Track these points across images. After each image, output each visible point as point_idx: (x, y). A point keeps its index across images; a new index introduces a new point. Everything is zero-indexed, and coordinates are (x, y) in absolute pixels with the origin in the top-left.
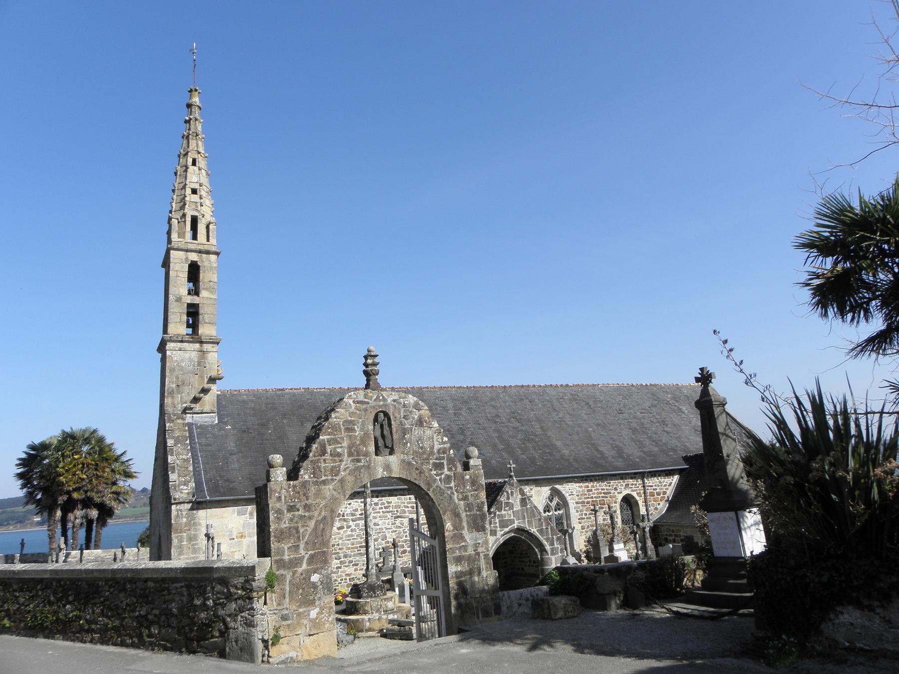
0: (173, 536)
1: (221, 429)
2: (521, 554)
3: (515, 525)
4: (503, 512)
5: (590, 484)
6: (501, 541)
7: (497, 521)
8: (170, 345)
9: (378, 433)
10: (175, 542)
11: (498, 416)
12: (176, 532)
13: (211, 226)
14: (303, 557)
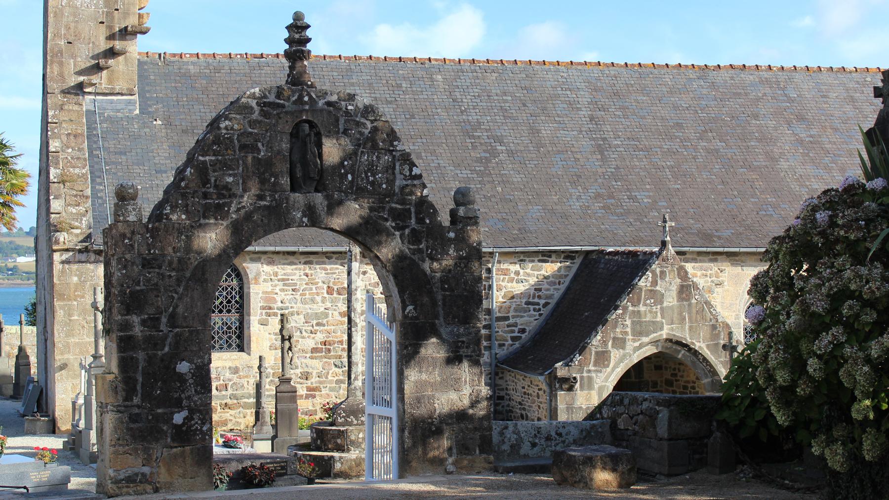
0: (57, 303)
3: (664, 333)
4: (642, 308)
7: (628, 322)
9: (296, 157)
10: (60, 314)
11: (679, 126)
12: (62, 297)
14: (166, 337)
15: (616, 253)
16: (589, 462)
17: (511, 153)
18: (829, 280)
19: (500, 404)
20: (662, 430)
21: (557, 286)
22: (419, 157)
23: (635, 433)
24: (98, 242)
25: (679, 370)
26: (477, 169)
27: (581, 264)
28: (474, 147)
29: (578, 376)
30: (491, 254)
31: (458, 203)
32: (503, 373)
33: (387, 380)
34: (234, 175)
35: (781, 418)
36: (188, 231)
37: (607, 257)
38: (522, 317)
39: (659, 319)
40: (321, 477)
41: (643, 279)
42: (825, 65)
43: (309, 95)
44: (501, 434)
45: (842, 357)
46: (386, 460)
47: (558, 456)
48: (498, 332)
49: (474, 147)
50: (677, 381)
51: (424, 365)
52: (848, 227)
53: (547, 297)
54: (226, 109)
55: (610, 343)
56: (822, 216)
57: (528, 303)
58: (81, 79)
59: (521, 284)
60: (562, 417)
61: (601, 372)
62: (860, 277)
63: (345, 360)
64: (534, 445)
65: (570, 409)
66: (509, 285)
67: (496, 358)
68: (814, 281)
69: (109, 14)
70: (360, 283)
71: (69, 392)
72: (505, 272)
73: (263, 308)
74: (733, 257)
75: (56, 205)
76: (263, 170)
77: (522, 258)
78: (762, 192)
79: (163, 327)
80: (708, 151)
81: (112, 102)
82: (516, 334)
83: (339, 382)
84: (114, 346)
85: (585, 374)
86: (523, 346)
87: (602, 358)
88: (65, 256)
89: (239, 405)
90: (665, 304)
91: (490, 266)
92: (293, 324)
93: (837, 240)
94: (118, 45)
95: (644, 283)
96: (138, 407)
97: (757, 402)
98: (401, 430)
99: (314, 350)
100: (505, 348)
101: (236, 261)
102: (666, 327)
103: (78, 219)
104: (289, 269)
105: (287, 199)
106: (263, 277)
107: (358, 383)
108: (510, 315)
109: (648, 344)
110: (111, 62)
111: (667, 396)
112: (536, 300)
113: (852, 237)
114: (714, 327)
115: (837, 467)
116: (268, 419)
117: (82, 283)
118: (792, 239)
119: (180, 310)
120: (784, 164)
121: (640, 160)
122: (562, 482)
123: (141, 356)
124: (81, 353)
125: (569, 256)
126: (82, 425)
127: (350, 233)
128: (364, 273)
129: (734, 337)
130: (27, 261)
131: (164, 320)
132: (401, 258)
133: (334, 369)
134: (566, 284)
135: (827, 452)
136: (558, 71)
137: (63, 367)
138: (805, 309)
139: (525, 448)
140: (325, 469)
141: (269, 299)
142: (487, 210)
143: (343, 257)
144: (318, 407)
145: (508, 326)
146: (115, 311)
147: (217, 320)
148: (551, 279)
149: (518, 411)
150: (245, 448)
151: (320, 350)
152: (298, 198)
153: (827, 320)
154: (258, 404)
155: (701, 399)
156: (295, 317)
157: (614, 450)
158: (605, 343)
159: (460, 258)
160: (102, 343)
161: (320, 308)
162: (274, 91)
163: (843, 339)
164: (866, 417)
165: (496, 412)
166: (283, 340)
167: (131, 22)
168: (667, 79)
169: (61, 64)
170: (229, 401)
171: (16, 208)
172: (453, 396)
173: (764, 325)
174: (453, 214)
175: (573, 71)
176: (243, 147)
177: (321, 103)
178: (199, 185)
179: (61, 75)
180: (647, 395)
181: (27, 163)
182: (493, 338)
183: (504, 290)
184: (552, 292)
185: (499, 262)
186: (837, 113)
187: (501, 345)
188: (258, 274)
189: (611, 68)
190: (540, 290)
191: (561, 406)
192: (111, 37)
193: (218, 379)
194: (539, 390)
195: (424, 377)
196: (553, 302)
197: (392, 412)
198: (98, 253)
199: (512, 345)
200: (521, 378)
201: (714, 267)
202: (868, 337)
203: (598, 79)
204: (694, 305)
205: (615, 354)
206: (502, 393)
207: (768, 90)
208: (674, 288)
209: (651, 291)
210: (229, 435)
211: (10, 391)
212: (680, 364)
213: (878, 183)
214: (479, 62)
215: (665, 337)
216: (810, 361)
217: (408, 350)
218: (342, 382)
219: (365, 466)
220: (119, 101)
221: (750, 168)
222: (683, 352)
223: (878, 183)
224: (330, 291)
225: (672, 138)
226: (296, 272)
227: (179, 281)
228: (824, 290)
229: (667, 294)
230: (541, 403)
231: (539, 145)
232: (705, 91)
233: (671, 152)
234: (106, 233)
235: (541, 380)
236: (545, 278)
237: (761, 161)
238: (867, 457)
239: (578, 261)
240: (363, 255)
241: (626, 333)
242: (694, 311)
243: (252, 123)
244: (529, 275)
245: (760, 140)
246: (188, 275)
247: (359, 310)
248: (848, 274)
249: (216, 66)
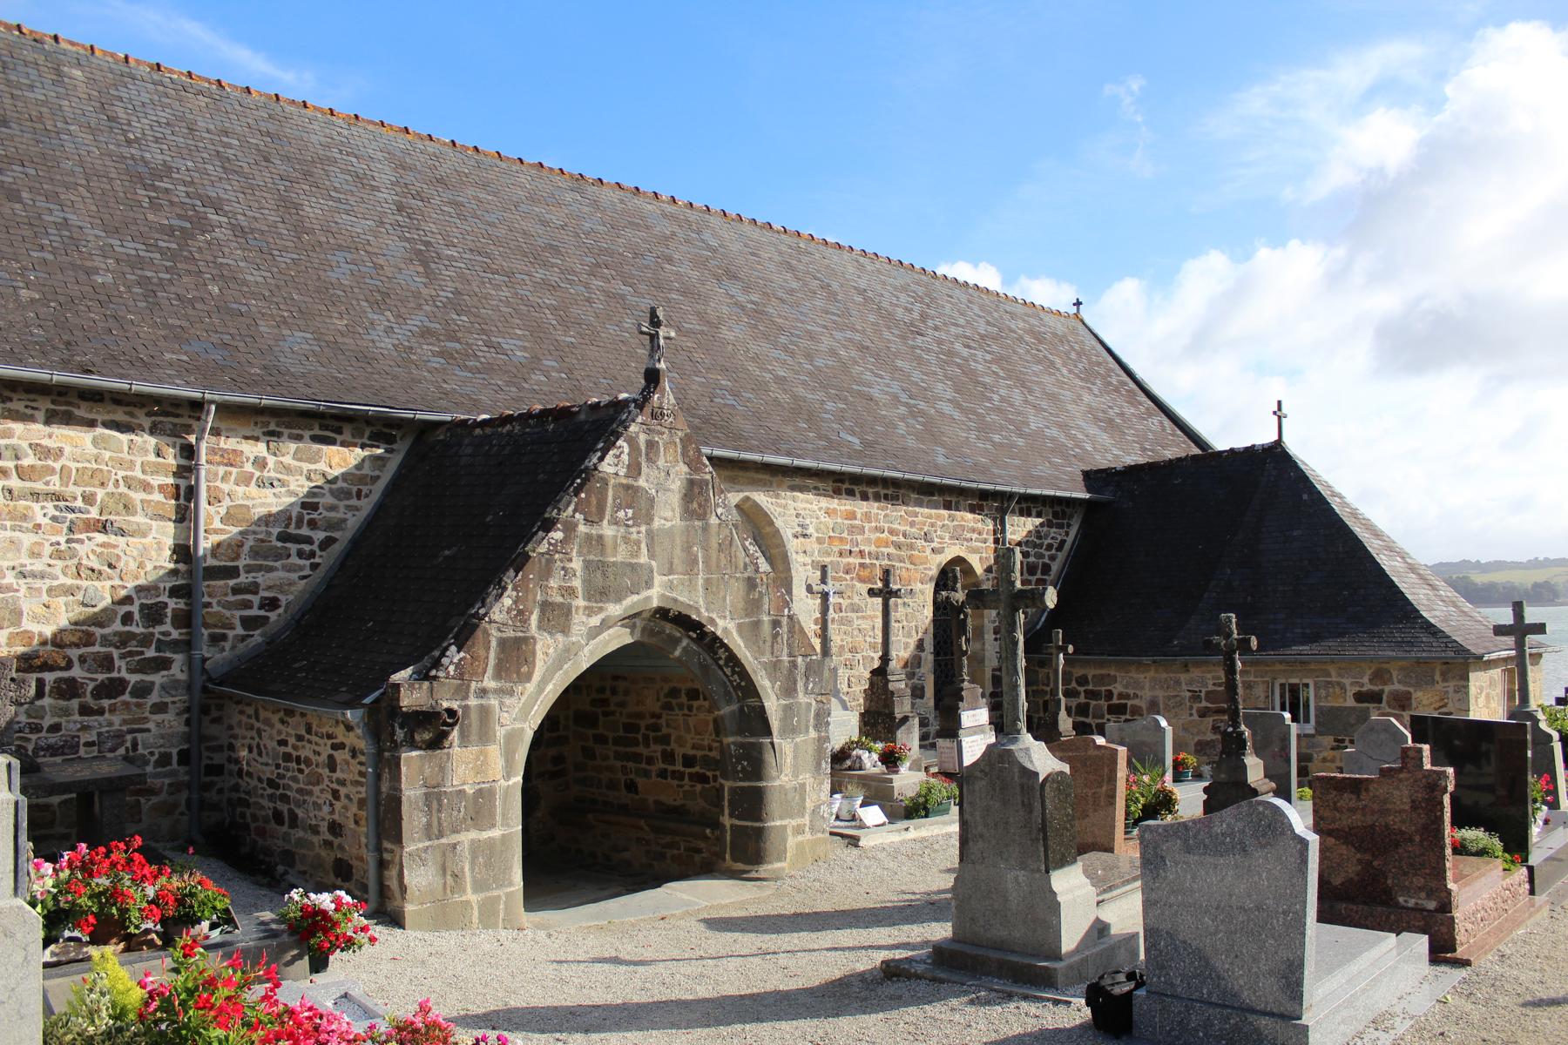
2: (631, 728)
3: (655, 596)
4: (608, 530)
5: (860, 507)
6: (585, 660)
7: (577, 564)
17: (238, 231)
19: (213, 784)
21: (354, 502)
25: (614, 691)
26: (161, 244)
27: (408, 454)
32: (220, 707)
37: (478, 431)
38: (271, 569)
41: (609, 458)
48: (209, 605)
49: (155, 205)
50: (606, 714)
53: (332, 525)
55: (534, 619)
57: (284, 537)
59: (269, 491)
61: (511, 693)
66: (241, 490)
67: (204, 671)
77: (272, 427)
82: (255, 612)
85: (473, 702)
86: (270, 641)
87: (515, 656)
90: (657, 523)
91: (192, 439)
95: (612, 466)
100: (227, 645)
108: (241, 563)
109: (615, 625)
112: (305, 531)
121: (497, 287)
125: (378, 429)
134: (376, 497)
142: (185, 324)
145: (235, 591)
148: (340, 484)
149: (265, 802)
158: (521, 616)
182: (198, 621)
183: (227, 502)
184: (340, 515)
185: (216, 432)
187: (216, 639)
189: (428, 143)
190: (314, 507)
194: (335, 747)
196: (344, 537)
199: (243, 638)
200: (275, 718)
203: (406, 152)
204: (714, 530)
205: (546, 647)
206: (218, 759)
208: (676, 485)
209: (628, 487)
212: (616, 678)
214: (171, 71)
215: (655, 604)
222: (685, 642)
225: (545, 264)
229: (661, 498)
230: (342, 783)
231: (300, 229)
233: (546, 285)
235: (349, 724)
241: (571, 592)
242: (714, 543)
244: (288, 469)
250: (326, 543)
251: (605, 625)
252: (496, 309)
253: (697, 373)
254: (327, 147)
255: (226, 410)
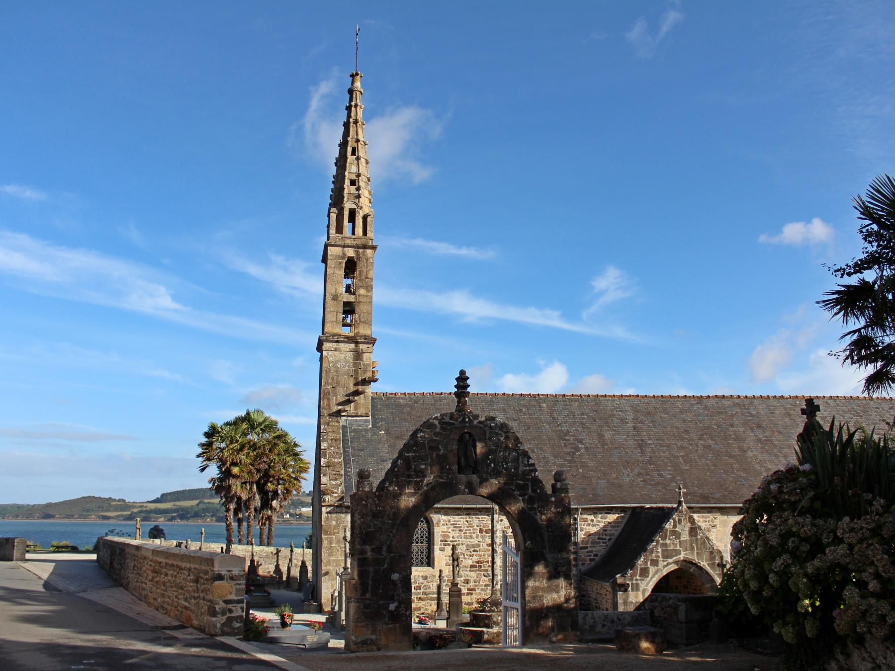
0: (323, 536)
1: (375, 434)
3: (682, 557)
7: (660, 550)
8: (326, 345)
10: (325, 543)
11: (687, 432)
13: (369, 219)
15: (651, 508)
16: (638, 637)
18: (780, 525)
20: (682, 617)
22: (533, 452)
23: (666, 619)
24: (348, 503)
28: (565, 446)
29: (630, 583)
30: (577, 509)
31: (556, 480)
33: (515, 582)
34: (425, 464)
35: (753, 610)
36: (397, 496)
39: (678, 548)
40: (476, 643)
42: (771, 394)
43: (469, 417)
44: (584, 619)
45: (790, 573)
46: (515, 634)
47: (619, 633)
49: (565, 446)
51: (537, 577)
52: (790, 493)
53: (611, 535)
54: (421, 426)
56: (773, 487)
57: (599, 539)
58: (340, 407)
60: (621, 608)
62: (798, 523)
63: (490, 572)
64: (604, 626)
65: (625, 603)
68: (770, 526)
69: (356, 372)
70: (499, 527)
71: (330, 588)
72: (585, 520)
73: (442, 541)
74: (723, 511)
75: (324, 480)
76: (442, 461)
78: (738, 471)
79: (384, 553)
80: (704, 446)
81: (356, 420)
83: (486, 585)
84: (356, 563)
87: (644, 572)
88: (329, 509)
89: (427, 599)
92: (459, 551)
93: (784, 501)
94: (360, 388)
95: (668, 526)
96: (369, 599)
97: (739, 600)
98: (523, 616)
99: (472, 566)
101: (427, 514)
102: (682, 553)
103: (336, 488)
104: (457, 518)
105: (456, 478)
106: (442, 522)
107: (498, 587)
110: (356, 398)
111: (684, 596)
113: (793, 499)
114: (712, 553)
115: (789, 641)
116: (444, 607)
117: (338, 525)
118: (756, 501)
119: (394, 543)
120: (750, 454)
121: (664, 452)
122: (621, 649)
123: (371, 569)
124: (337, 566)
125: (623, 510)
126: (337, 608)
127: (492, 497)
128: (501, 520)
129: (725, 559)
130: (307, 510)
131: (384, 549)
132: (522, 512)
133: (483, 578)
135: (783, 631)
136: (614, 400)
137: (327, 573)
138: (766, 542)
139: (599, 628)
140: (478, 638)
141: (445, 537)
143: (489, 512)
144: (474, 601)
146: (357, 543)
147: (415, 547)
150: (431, 625)
151: (475, 566)
152: (463, 478)
153: (780, 550)
154: (439, 599)
155: (704, 598)
156: (461, 546)
157: (652, 629)
158: (646, 563)
159: (558, 513)
160: (349, 561)
161: (475, 541)
162: (449, 415)
163: (790, 562)
164: (807, 611)
165: (580, 604)
166: (454, 560)
167: (368, 375)
168: (679, 404)
169: (329, 399)
170: (422, 596)
171: (302, 481)
172: (555, 596)
173: (742, 553)
174: (553, 486)
175: (623, 401)
176: (431, 448)
177: (475, 422)
178: (403, 470)
179: (329, 405)
180: (672, 595)
181: (309, 455)
186: (780, 423)
188: (439, 521)
191: (620, 601)
192: (356, 384)
193: (415, 583)
195: (537, 584)
196: (614, 538)
197: (518, 605)
198: (348, 507)
201: (710, 516)
202: (806, 560)
203: (638, 405)
205: (652, 569)
206: (584, 593)
207: (738, 410)
208: (687, 529)
210: (422, 616)
211: (296, 586)
213: (807, 467)
216: (771, 575)
217: (527, 572)
218: (488, 585)
219: (502, 637)
220: (360, 420)
221: (731, 456)
223: (807, 467)
224: (481, 531)
225: (683, 439)
226: (461, 520)
227: (393, 525)
228: (777, 532)
229: (682, 533)
231: (604, 444)
232: (701, 411)
234: (353, 497)
235: (607, 586)
236: (609, 523)
237: (736, 452)
238: (809, 635)
239: (629, 513)
240: (500, 510)
243: (436, 434)
245: (734, 440)
246: (398, 522)
247: (498, 543)
248: (791, 522)
249: (415, 400)
250: (609, 540)
251: (668, 564)
252: (663, 461)
253: (733, 473)
254: (612, 410)
255: (583, 509)
